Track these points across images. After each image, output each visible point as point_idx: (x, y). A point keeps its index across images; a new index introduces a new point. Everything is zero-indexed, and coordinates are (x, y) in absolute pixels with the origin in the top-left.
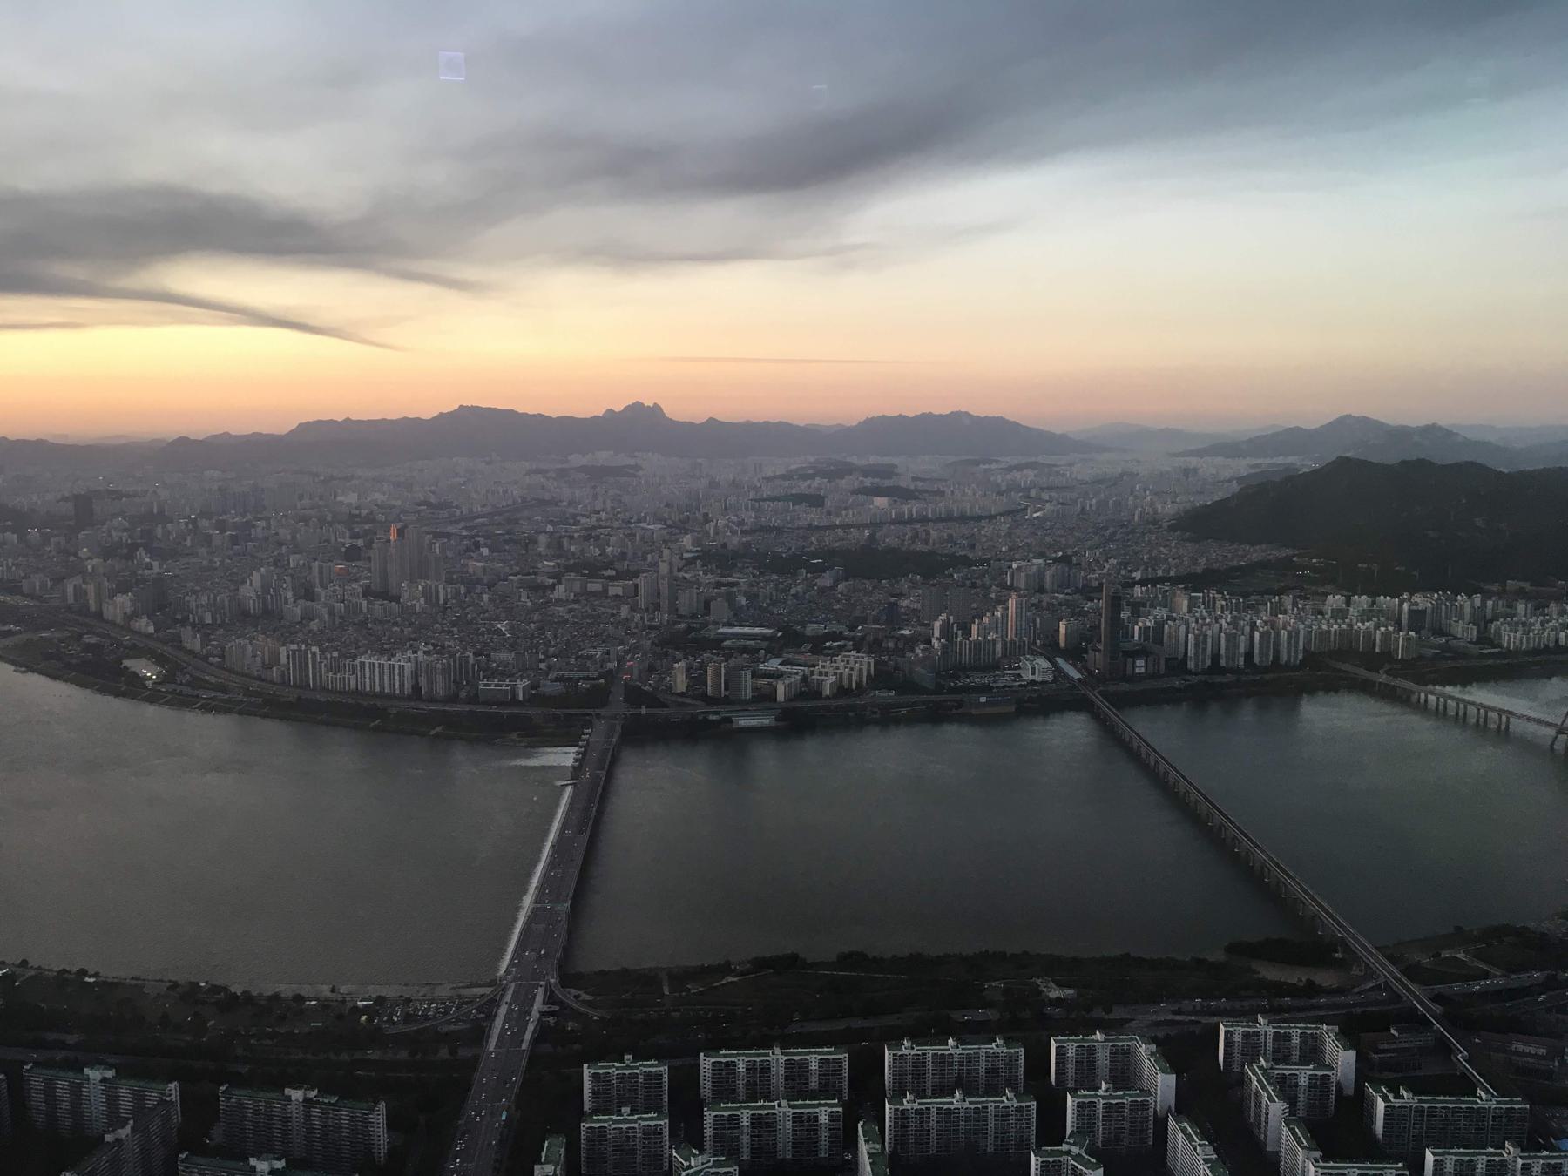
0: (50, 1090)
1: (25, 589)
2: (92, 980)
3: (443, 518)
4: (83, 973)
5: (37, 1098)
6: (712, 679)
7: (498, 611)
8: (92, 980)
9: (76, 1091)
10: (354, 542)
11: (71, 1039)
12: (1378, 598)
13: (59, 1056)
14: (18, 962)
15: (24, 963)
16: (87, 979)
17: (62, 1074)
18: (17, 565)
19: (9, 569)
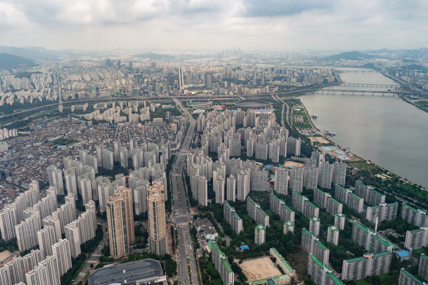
0: (408, 210)
1: (423, 88)
2: (423, 189)
3: (236, 108)
4: (421, 187)
5: (404, 212)
6: (26, 109)
7: (103, 83)
8: (423, 189)
9: (414, 214)
10: (111, 94)
11: (415, 201)
12: (124, 167)
13: (411, 204)
14: (405, 179)
15: (406, 180)
16: (421, 189)
17: (412, 208)
18: (422, 82)
19: (420, 82)
